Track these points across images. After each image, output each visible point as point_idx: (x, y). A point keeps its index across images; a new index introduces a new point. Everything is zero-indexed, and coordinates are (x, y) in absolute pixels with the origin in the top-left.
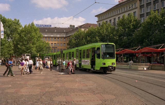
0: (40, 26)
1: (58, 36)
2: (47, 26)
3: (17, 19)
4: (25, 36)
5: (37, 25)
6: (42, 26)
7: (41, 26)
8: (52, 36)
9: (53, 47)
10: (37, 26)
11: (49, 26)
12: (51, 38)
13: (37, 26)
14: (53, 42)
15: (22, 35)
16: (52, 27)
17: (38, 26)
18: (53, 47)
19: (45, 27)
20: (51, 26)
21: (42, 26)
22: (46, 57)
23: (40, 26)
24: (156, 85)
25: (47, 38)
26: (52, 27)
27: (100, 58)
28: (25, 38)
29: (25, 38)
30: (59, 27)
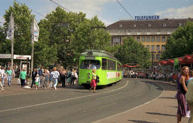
0: (141, 18)
1: (138, 34)
2: (153, 17)
3: (84, 13)
4: (83, 37)
5: (136, 17)
6: (144, 18)
7: (142, 18)
8: (158, 33)
9: (159, 52)
10: (137, 19)
11: (155, 17)
12: (156, 37)
13: (137, 19)
14: (156, 44)
15: (78, 35)
16: (160, 18)
17: (138, 18)
18: (159, 52)
19: (149, 19)
20: (158, 17)
21: (144, 18)
22: (28, 66)
23: (141, 18)
24: (131, 121)
25: (151, 37)
26: (160, 18)
27: (115, 70)
28: (82, 39)
29: (82, 39)
30: (172, 18)
